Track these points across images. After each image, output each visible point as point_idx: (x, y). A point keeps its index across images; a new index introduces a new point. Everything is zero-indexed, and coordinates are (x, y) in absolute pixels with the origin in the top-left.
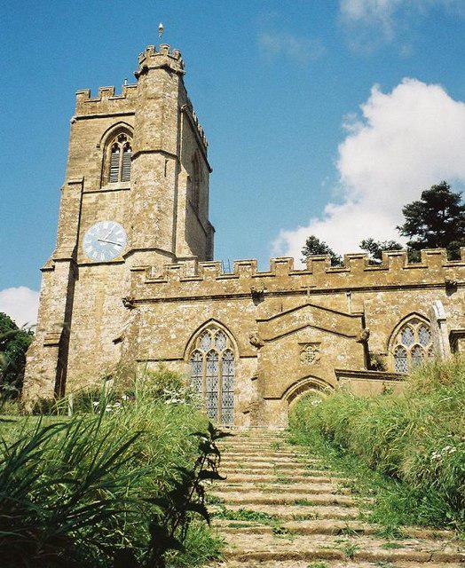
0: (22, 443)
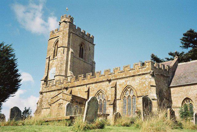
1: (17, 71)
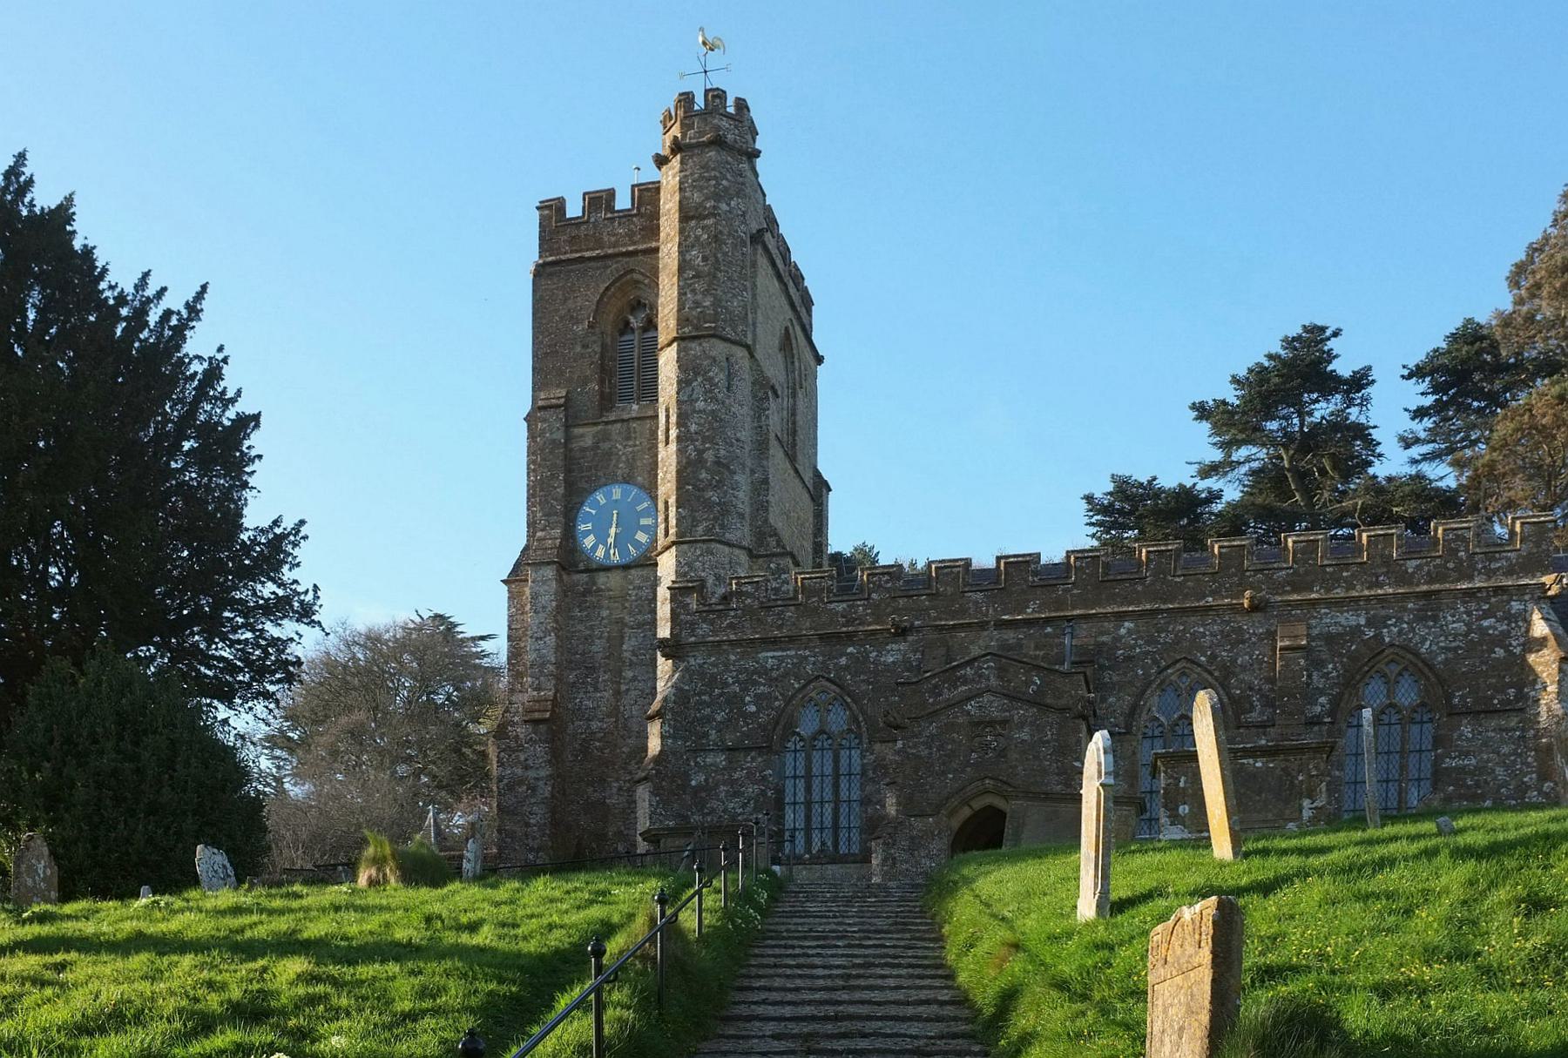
0: (922, 1042)
1: (1270, 357)
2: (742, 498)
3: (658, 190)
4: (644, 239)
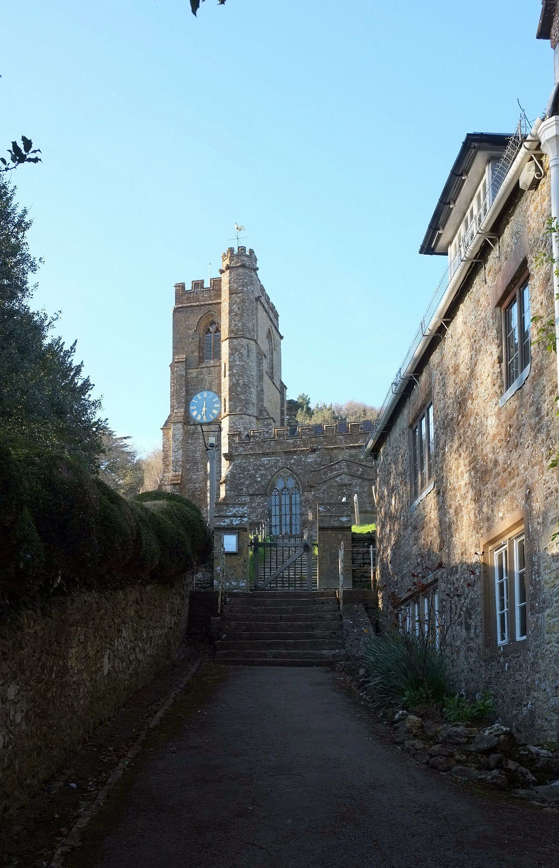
2: (254, 398)
3: (220, 281)
4: (215, 299)
